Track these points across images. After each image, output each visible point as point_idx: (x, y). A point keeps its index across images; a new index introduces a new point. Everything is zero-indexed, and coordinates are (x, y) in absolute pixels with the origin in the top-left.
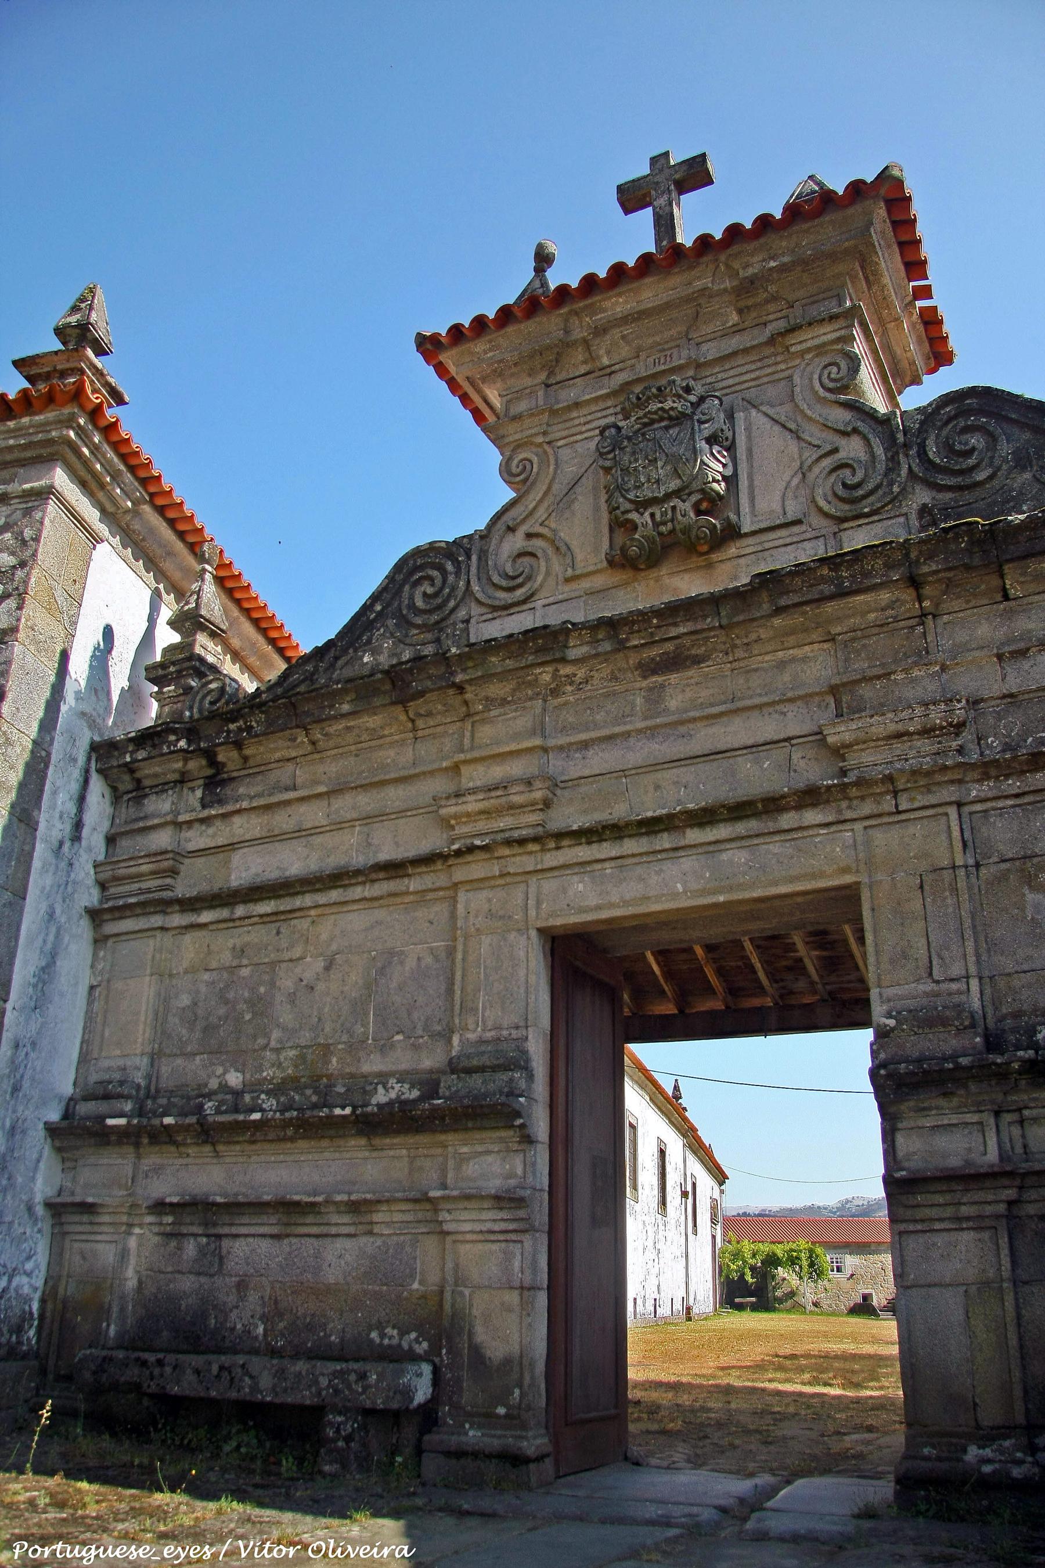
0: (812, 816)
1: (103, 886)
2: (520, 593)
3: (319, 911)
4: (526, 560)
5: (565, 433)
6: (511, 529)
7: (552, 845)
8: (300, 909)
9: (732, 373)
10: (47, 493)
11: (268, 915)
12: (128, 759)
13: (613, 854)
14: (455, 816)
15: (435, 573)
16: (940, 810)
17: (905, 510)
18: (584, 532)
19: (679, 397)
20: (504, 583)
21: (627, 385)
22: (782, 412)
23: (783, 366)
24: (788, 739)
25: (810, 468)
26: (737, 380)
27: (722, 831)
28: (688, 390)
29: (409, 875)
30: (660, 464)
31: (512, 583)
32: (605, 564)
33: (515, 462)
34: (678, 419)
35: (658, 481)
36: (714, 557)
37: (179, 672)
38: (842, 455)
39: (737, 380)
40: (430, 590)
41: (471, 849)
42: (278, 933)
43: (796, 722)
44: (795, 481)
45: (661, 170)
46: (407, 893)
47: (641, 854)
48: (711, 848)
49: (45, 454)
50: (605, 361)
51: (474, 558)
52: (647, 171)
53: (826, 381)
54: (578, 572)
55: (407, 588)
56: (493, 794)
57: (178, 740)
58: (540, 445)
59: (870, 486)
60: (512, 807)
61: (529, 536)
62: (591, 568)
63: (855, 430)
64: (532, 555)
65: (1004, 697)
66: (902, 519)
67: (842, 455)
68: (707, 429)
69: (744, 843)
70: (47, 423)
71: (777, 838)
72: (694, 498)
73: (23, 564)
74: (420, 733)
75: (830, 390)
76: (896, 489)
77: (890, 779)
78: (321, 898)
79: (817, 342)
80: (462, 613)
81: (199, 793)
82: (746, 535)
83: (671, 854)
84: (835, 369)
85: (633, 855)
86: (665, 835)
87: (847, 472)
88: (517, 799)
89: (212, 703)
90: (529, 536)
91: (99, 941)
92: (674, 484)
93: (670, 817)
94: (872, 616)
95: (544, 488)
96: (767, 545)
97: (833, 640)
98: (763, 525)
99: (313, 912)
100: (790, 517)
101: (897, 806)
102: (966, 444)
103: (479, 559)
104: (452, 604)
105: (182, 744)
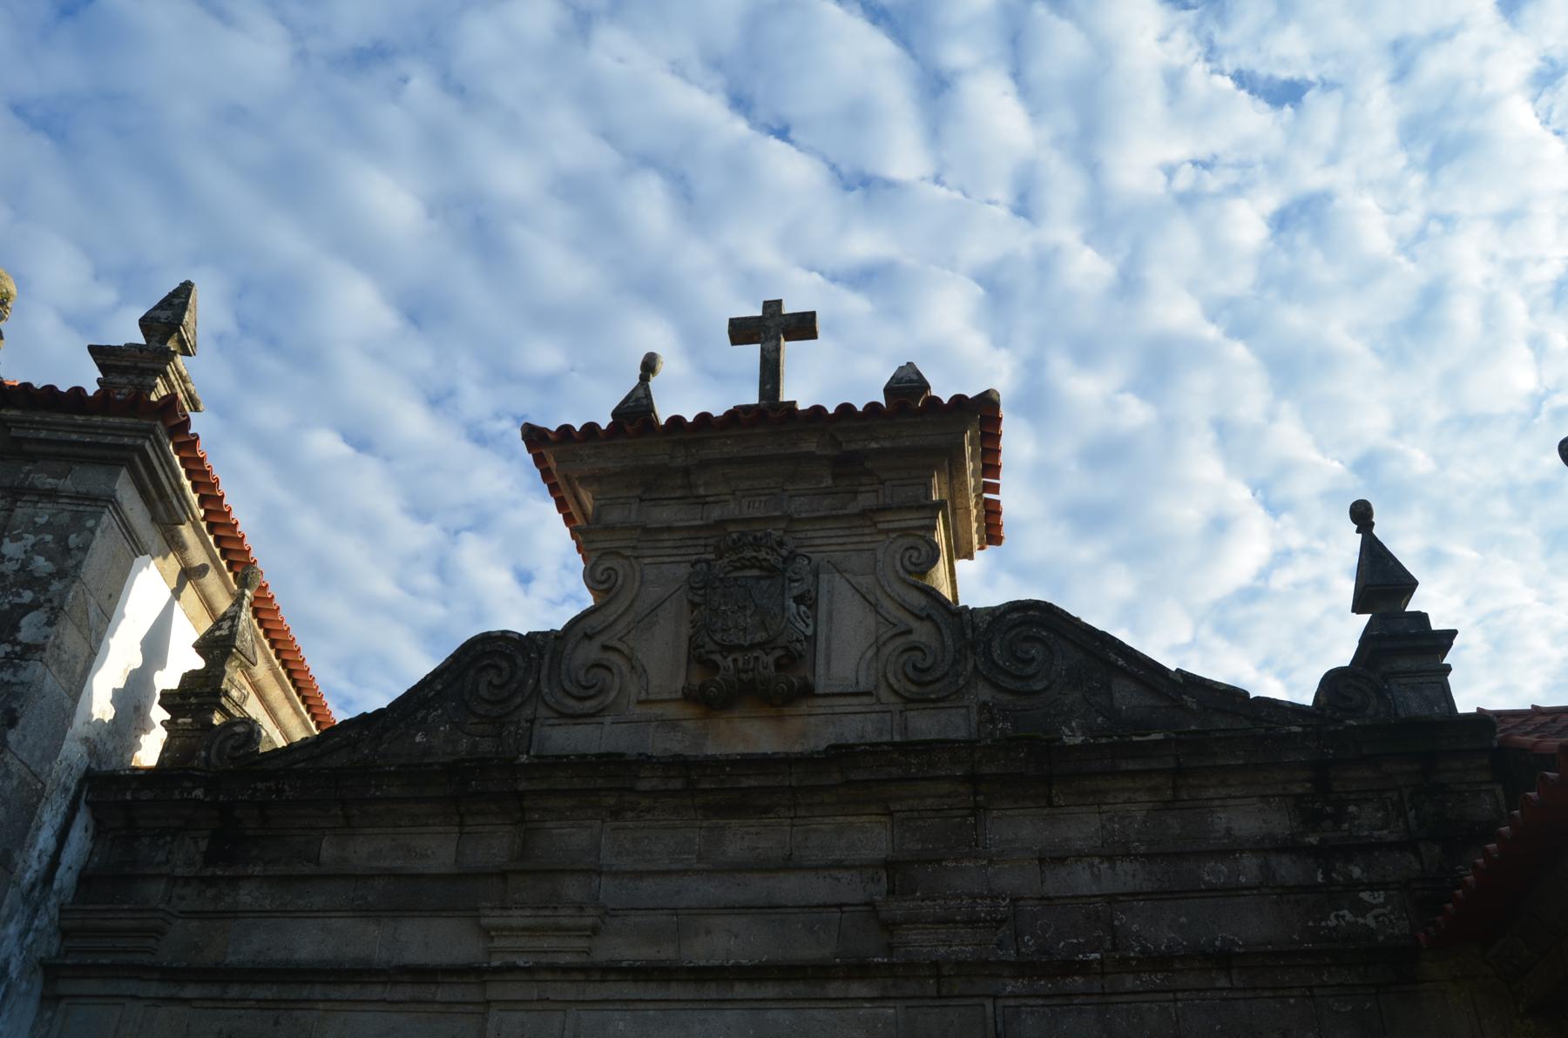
0: (858, 989)
1: (65, 933)
2: (590, 705)
3: (328, 1006)
4: (602, 673)
5: (654, 552)
6: (588, 637)
7: (597, 976)
8: (306, 1001)
9: (821, 533)
10: (111, 501)
11: (267, 1001)
12: (129, 797)
13: (658, 996)
14: (497, 929)
15: (504, 664)
16: (976, 1000)
17: (966, 703)
18: (662, 657)
19: (773, 549)
20: (575, 691)
21: (721, 524)
22: (865, 581)
23: (868, 539)
24: (840, 906)
25: (884, 644)
26: (825, 541)
27: (771, 990)
28: (781, 544)
29: (437, 983)
30: (748, 613)
31: (583, 693)
32: (679, 695)
33: (601, 568)
34: (771, 571)
35: (745, 629)
36: (786, 711)
37: (200, 705)
38: (913, 637)
39: (825, 541)
40: (496, 681)
41: (512, 968)
42: (276, 1023)
43: (850, 889)
44: (870, 654)
45: (772, 316)
46: (433, 1002)
47: (686, 1001)
48: (756, 1005)
49: (115, 457)
50: (702, 491)
51: (547, 657)
52: (759, 313)
53: (907, 563)
54: (652, 697)
55: (472, 672)
56: (542, 912)
57: (194, 789)
58: (627, 558)
59: (938, 674)
60: (558, 929)
61: (605, 648)
62: (666, 696)
63: (929, 617)
64: (608, 669)
65: (1042, 898)
66: (963, 711)
67: (913, 637)
68: (797, 588)
69: (790, 1005)
70: (122, 428)
71: (822, 1004)
72: (779, 653)
73: (61, 574)
74: (467, 829)
75: (903, 566)
76: (961, 682)
77: (936, 965)
78: (334, 993)
79: (903, 524)
80: (527, 712)
81: (203, 845)
82: (819, 696)
83: (717, 1005)
84: (915, 554)
85: (679, 1001)
86: (713, 985)
87: (919, 653)
88: (565, 921)
89: (233, 748)
90: (605, 648)
91: (49, 999)
92: (760, 636)
93: (722, 968)
94: (929, 801)
95: (627, 603)
96: (837, 710)
97: (891, 814)
98: (836, 690)
99: (321, 1006)
100: (862, 687)
101: (939, 991)
102: (1027, 652)
103: (552, 659)
104: (518, 700)
105: (199, 793)
